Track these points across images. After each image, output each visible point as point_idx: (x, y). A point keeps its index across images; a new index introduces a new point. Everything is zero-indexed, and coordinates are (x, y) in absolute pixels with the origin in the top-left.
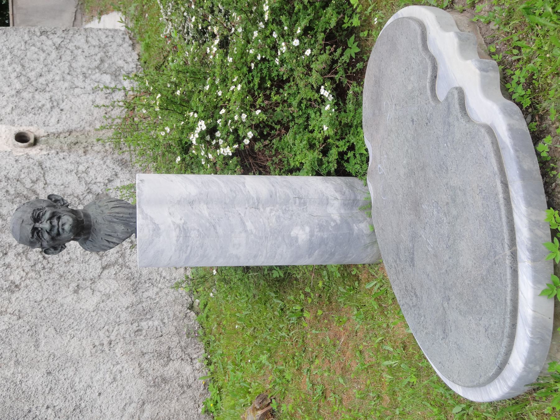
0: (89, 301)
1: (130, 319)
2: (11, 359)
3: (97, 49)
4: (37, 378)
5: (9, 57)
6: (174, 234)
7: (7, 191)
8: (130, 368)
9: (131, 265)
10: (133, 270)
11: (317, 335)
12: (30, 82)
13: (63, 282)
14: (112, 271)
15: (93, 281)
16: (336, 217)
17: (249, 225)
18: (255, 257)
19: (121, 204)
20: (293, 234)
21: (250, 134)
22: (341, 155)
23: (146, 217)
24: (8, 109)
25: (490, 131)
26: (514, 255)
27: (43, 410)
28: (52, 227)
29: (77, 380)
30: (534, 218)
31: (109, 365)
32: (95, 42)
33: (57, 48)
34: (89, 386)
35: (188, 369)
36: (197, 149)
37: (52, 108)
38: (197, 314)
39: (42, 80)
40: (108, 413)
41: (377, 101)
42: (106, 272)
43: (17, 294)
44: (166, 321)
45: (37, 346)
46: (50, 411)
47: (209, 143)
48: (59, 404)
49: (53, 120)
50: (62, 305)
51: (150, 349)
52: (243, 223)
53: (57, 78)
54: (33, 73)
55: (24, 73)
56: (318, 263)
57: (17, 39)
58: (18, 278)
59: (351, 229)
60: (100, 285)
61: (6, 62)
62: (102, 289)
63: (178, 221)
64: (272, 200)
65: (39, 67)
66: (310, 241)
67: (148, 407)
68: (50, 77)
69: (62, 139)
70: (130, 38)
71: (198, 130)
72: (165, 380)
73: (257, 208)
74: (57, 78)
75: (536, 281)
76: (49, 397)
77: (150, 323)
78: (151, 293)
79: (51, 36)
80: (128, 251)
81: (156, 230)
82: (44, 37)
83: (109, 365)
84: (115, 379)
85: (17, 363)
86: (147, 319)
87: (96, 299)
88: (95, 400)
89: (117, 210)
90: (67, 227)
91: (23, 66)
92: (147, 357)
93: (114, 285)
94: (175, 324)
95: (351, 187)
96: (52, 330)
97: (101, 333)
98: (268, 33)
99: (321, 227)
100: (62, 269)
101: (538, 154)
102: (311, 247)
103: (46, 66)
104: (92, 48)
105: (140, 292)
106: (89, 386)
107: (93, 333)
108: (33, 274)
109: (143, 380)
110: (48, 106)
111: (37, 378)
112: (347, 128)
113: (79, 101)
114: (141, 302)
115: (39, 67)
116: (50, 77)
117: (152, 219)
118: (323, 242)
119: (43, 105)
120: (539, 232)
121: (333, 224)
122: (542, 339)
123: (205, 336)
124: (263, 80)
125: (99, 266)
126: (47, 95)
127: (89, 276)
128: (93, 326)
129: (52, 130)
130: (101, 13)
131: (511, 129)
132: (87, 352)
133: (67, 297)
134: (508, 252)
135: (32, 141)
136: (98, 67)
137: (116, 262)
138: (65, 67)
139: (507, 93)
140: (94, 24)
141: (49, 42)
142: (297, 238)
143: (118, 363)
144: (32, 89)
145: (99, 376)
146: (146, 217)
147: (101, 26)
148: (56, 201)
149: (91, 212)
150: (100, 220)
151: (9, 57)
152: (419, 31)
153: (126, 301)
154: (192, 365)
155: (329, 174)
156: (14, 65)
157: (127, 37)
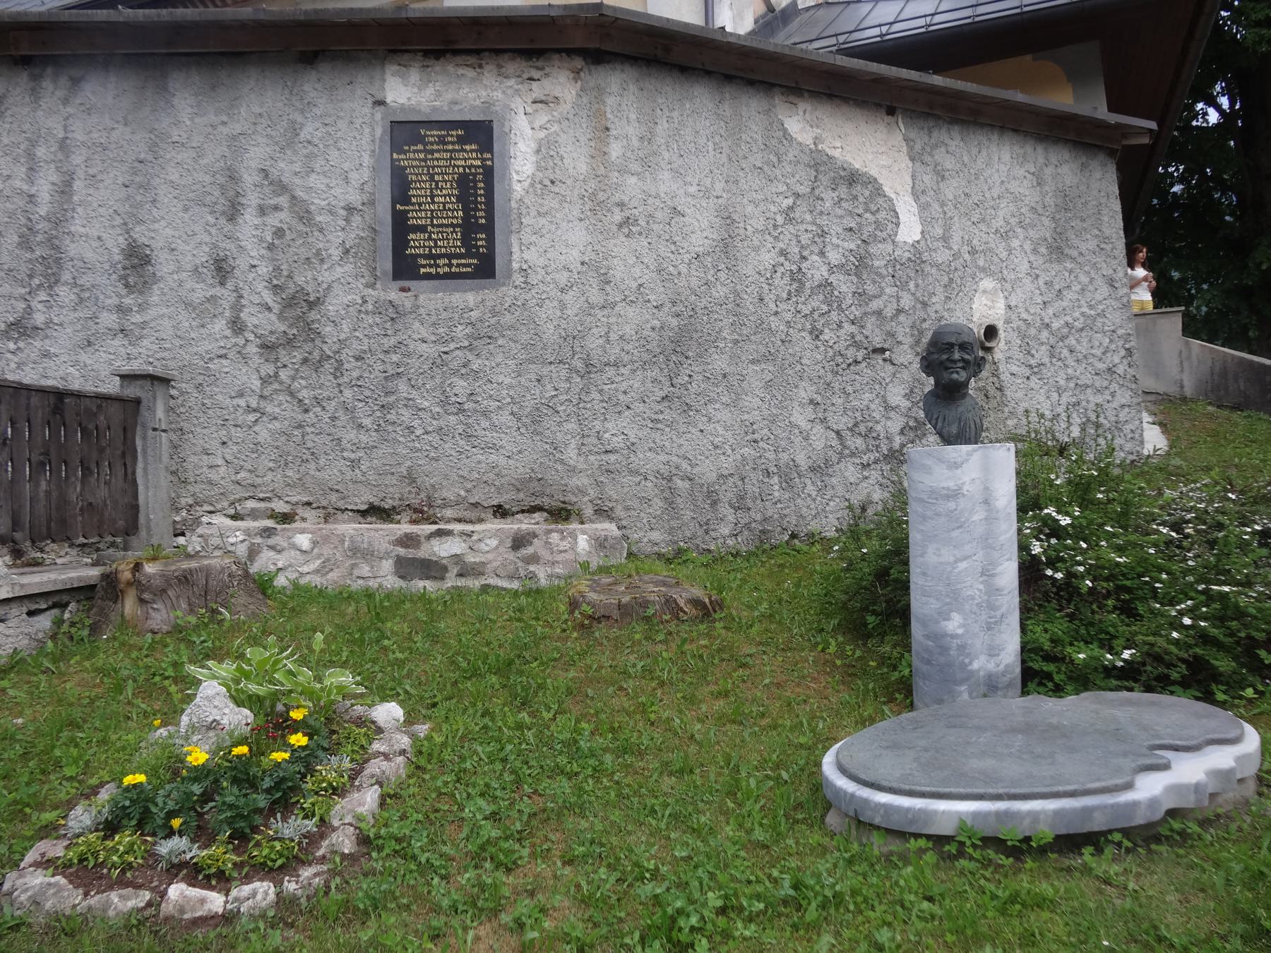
0: (800, 417)
1: (781, 463)
2: (740, 335)
3: (1114, 419)
4: (720, 363)
5: (1092, 312)
6: (951, 484)
7: (925, 320)
8: (727, 464)
9: (842, 465)
10: (837, 467)
11: (807, 660)
12: (1063, 338)
13: (822, 387)
14: (835, 443)
15: (823, 420)
16: (975, 665)
17: (963, 565)
18: (924, 574)
19: (980, 429)
20: (954, 615)
21: (1059, 575)
22: (1049, 676)
23: (969, 454)
24: (1024, 316)
25: (1129, 786)
26: (998, 797)
27: (688, 372)
28: (955, 362)
29: (717, 406)
30: (1042, 817)
31: (732, 441)
32: (1123, 415)
33: (1109, 369)
34: (710, 419)
35: (726, 531)
36: (1034, 517)
37: (1030, 367)
38: (787, 542)
39: (1065, 352)
40: (681, 441)
41: (1129, 703)
42: (834, 435)
43: (808, 338)
44: (779, 506)
45: (753, 362)
46: (687, 378)
47: (1041, 532)
48: (694, 388)
49: (1014, 369)
50: (796, 387)
51: (748, 487)
52: (965, 558)
53: (1070, 371)
54: (1074, 342)
55: (265, 419)
56: (914, 646)
57: (1118, 321)
58: (827, 338)
59: (962, 682)
60: (818, 429)
61: (1085, 309)
62: (814, 431)
63: (965, 488)
64: (992, 591)
65: (1082, 348)
66: (945, 635)
67: (687, 484)
68: (1071, 362)
69: (991, 380)
70: (1132, 462)
71: (1059, 517)
72: (714, 503)
73: (982, 574)
74: (1070, 371)
75: (976, 815)
76: (701, 377)
77: (777, 487)
78: (810, 489)
79: (1125, 362)
80: (858, 461)
81: (956, 466)
82: (1123, 353)
83: (732, 441)
84: (716, 447)
85: (736, 342)
86: (781, 483)
87: (803, 424)
88: (695, 426)
89: (973, 426)
90: (955, 376)
91: (1082, 330)
92: (740, 483)
93: (819, 445)
94: (776, 516)
95: (1010, 685)
96: (770, 376)
97: (766, 431)
98: (1193, 594)
99: (962, 648)
100: (836, 385)
101: (1110, 831)
102: (939, 638)
103: (1085, 357)
104: (1114, 412)
105: (811, 475)
106: (710, 419)
107: (766, 422)
108: (831, 354)
109: (715, 479)
110: (1033, 362)
111: (720, 363)
112: (1083, 680)
113: (1042, 399)
114: (800, 476)
115: (1082, 348)
116: (1071, 362)
117: (967, 460)
118: (944, 650)
119: (1033, 356)
120: (1027, 822)
121: (967, 661)
122: (912, 822)
123: (763, 548)
124: (1128, 590)
125: (841, 426)
126: (1046, 360)
127: (829, 415)
128: (773, 422)
129: (1002, 368)
130: (1161, 425)
131: (1135, 804)
132: (746, 417)
133: (805, 391)
134: (1001, 791)
135: (988, 344)
136: (1088, 420)
137: (845, 447)
138: (1086, 379)
139: (1172, 813)
140: (1146, 418)
141: (1117, 360)
142: (948, 619)
143: (733, 450)
144: (1052, 341)
145: (720, 430)
146: (969, 454)
147: (1145, 425)
148: (979, 366)
149: (967, 399)
150: (961, 409)
151: (1092, 312)
152: (1229, 736)
153: (801, 459)
154: (730, 536)
155: (1023, 662)
156: (1082, 320)
157: (1131, 457)
